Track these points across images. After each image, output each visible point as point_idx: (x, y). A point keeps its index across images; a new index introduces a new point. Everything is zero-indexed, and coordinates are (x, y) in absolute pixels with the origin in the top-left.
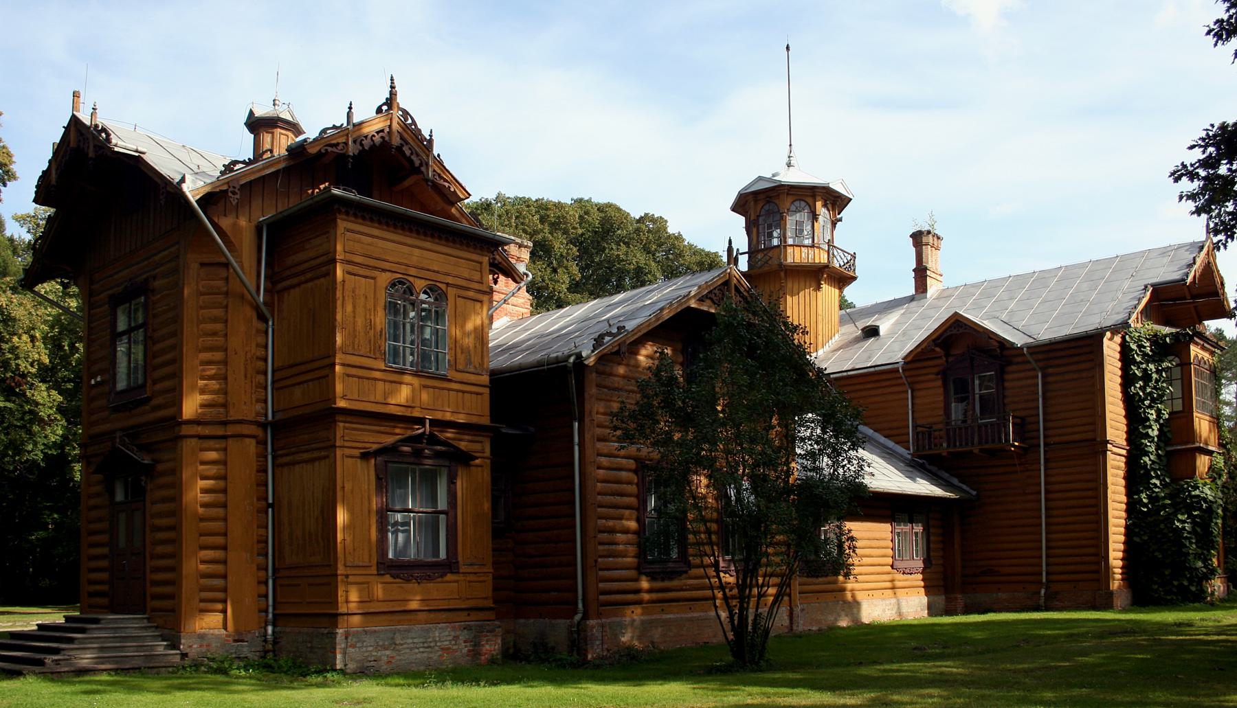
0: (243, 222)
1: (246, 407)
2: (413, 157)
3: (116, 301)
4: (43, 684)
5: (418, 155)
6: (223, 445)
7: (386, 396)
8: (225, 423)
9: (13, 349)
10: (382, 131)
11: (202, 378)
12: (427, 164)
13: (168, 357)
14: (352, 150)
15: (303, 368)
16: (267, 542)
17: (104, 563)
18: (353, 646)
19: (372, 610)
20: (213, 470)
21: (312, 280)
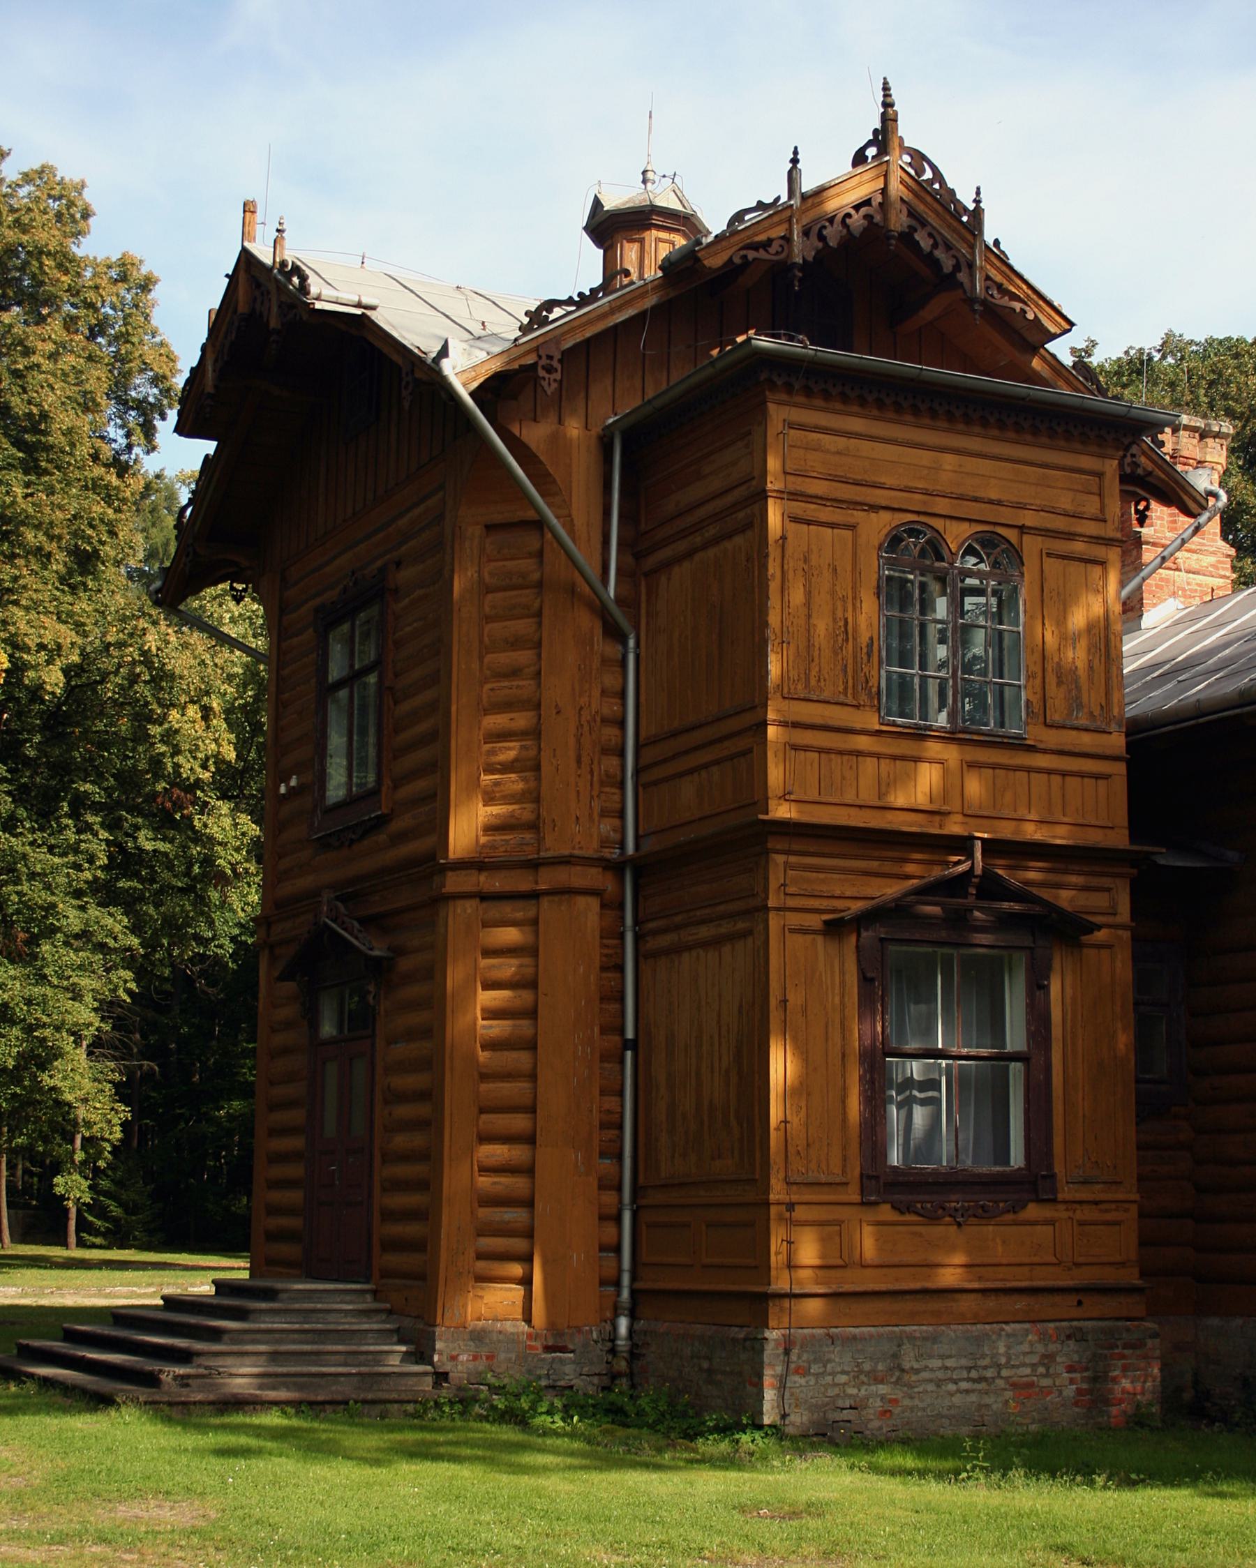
0: (574, 429)
1: (579, 830)
2: (939, 254)
3: (328, 619)
4: (149, 1428)
5: (949, 247)
6: (531, 913)
7: (883, 787)
8: (534, 865)
9: (169, 735)
10: (867, 203)
11: (490, 770)
12: (971, 265)
13: (422, 728)
14: (801, 250)
15: (698, 737)
16: (621, 1127)
17: (295, 1171)
18: (803, 1371)
19: (847, 1288)
20: (508, 968)
21: (716, 541)
